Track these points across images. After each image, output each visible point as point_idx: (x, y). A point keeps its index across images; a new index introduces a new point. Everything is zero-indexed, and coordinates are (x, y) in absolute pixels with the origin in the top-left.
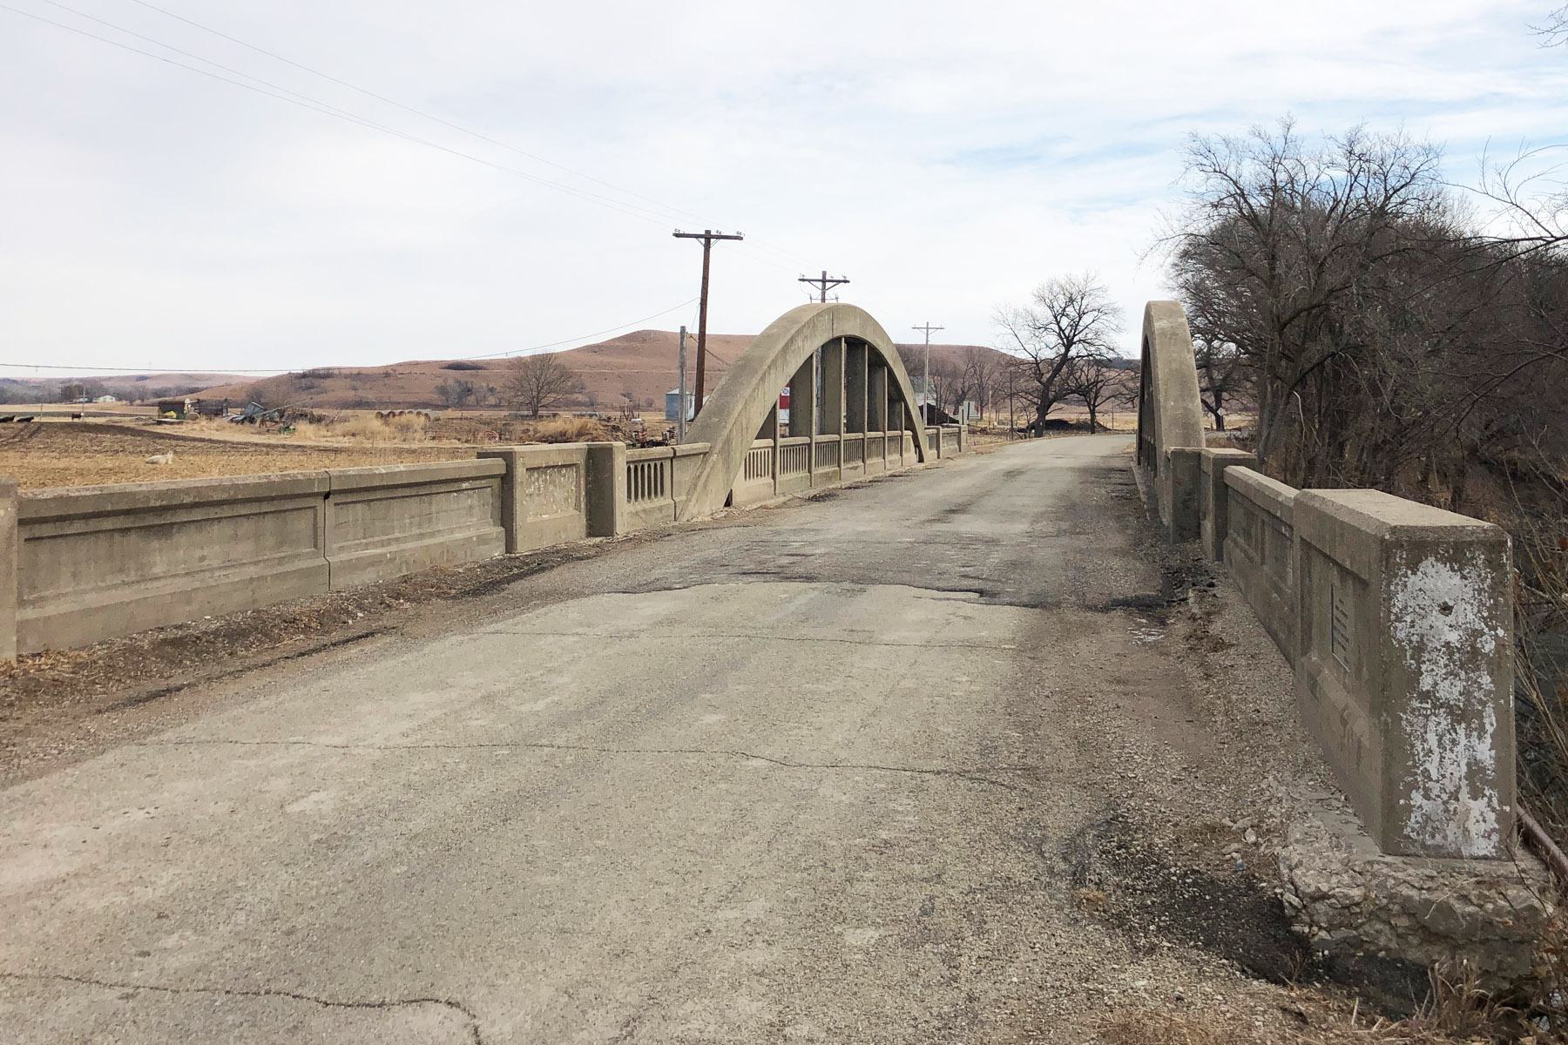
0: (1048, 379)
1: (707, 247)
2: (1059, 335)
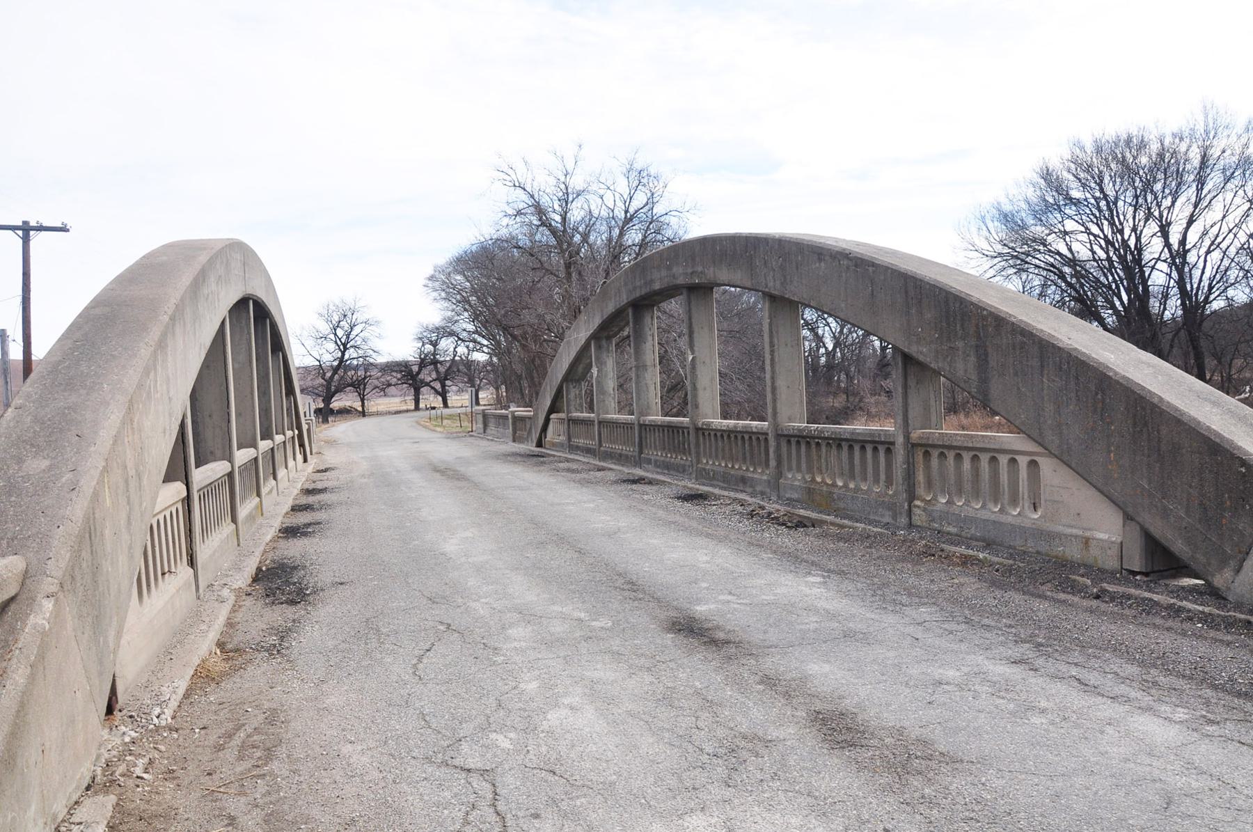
0: (330, 378)
1: (26, 241)
2: (336, 342)
